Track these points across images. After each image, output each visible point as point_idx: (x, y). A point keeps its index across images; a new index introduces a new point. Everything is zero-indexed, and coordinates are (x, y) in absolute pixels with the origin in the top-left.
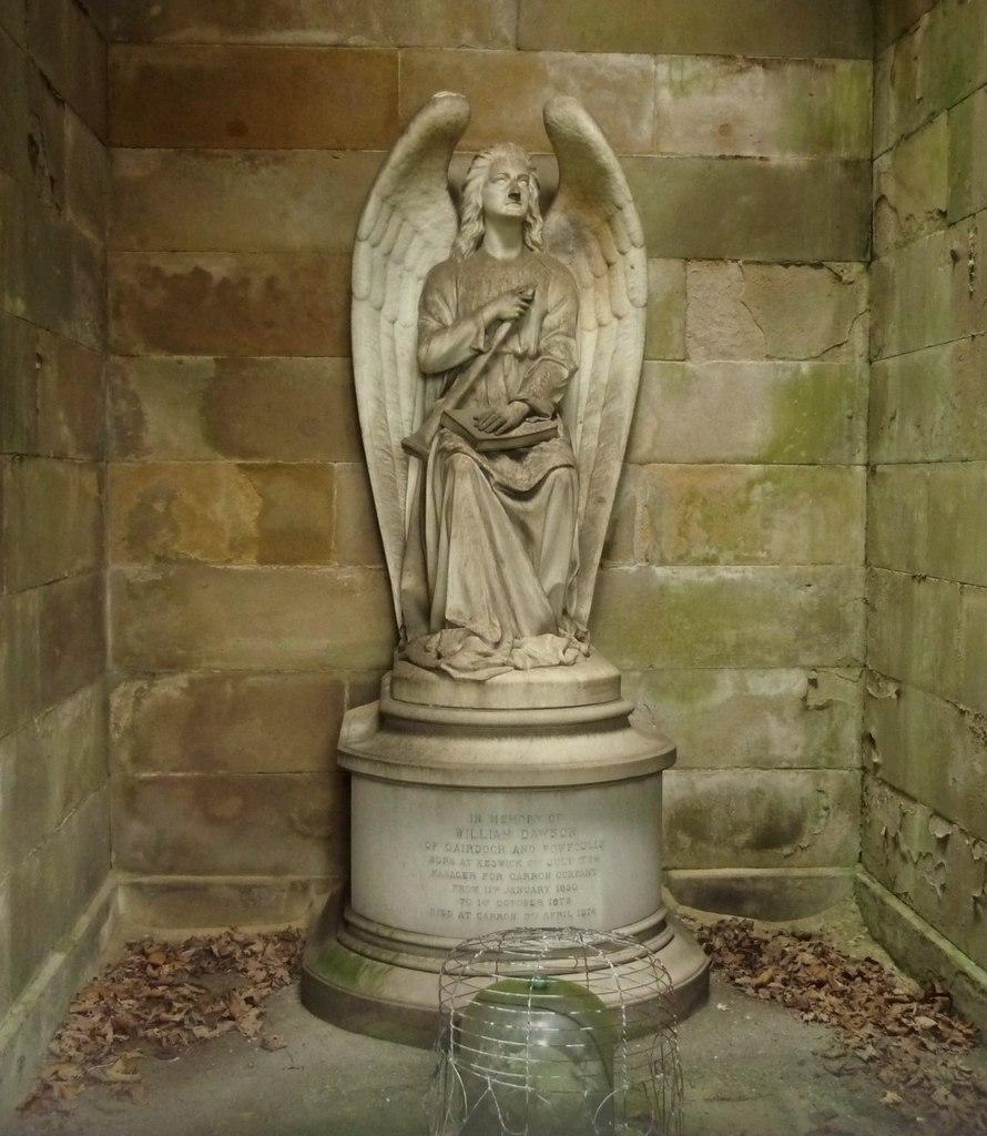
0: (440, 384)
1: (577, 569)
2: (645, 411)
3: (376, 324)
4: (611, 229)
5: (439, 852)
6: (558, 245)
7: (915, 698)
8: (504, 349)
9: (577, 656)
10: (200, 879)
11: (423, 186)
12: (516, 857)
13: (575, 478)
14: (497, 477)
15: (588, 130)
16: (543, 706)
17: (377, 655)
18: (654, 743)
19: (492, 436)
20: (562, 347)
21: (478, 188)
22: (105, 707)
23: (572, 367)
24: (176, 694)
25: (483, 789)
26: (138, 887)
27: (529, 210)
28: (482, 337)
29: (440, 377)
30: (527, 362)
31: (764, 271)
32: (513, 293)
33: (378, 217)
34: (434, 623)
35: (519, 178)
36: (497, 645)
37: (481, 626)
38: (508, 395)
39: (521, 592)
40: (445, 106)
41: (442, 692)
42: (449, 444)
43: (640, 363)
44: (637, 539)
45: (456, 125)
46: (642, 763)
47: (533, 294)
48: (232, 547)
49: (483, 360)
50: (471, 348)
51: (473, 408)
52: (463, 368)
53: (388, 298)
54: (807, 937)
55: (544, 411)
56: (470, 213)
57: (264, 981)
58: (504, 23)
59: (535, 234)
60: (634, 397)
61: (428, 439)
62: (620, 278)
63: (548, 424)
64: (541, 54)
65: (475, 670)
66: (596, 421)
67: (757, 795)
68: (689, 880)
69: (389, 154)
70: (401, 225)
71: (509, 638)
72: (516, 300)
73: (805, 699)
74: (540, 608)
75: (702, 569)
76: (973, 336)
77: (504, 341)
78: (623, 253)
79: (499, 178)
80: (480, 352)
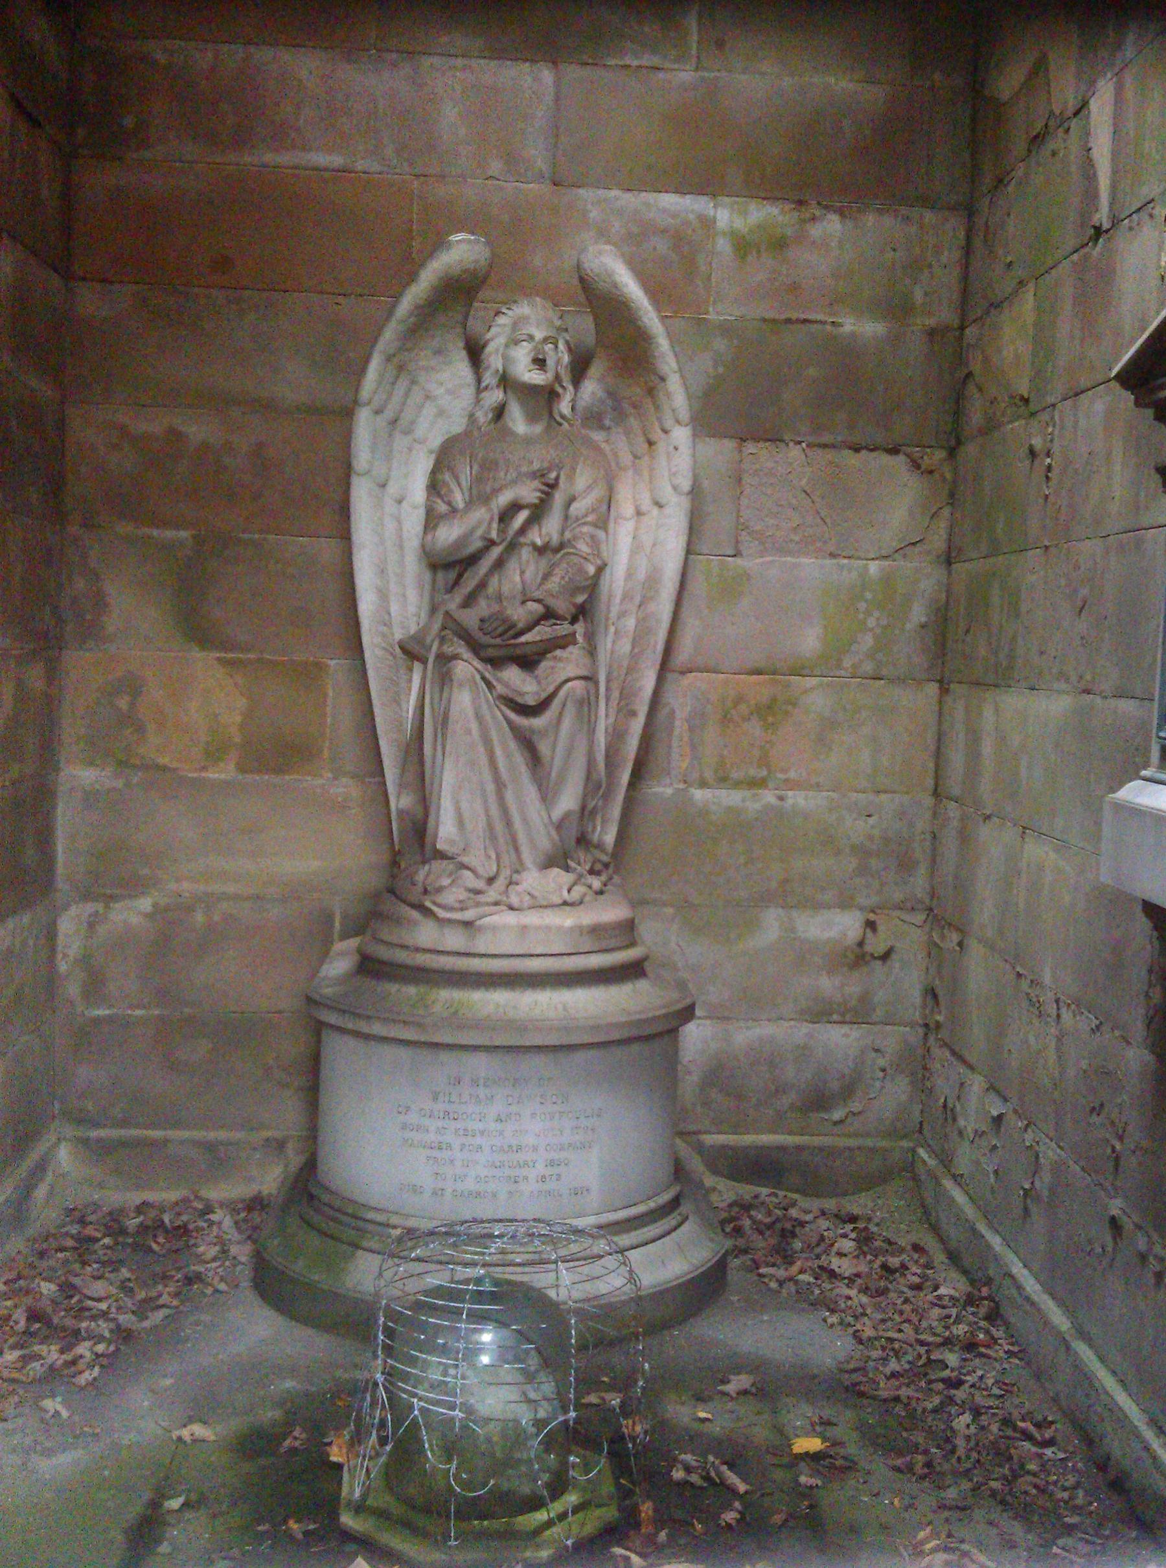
0: (452, 575)
1: (596, 789)
2: (686, 612)
3: (379, 505)
4: (654, 404)
5: (413, 1118)
6: (594, 419)
7: (976, 950)
8: (522, 540)
9: (585, 895)
10: (158, 1134)
11: (435, 343)
12: (500, 1126)
13: (592, 692)
14: (500, 689)
15: (627, 285)
16: (538, 952)
17: (375, 880)
18: (675, 995)
19: (498, 641)
20: (588, 540)
21: (497, 350)
22: (51, 934)
23: (599, 562)
24: (134, 920)
25: (464, 1048)
26: (85, 1142)
27: (557, 378)
28: (495, 525)
29: (451, 568)
30: (549, 555)
31: (830, 455)
32: (534, 475)
33: (381, 376)
34: (428, 854)
35: (546, 340)
36: (491, 880)
37: (473, 859)
38: (524, 592)
39: (525, 820)
40: (462, 251)
41: (425, 934)
42: (448, 649)
43: (682, 558)
44: (677, 755)
45: (474, 273)
46: (655, 1019)
47: (557, 479)
48: (207, 753)
49: (496, 552)
50: (484, 538)
51: (483, 608)
52: (473, 560)
53: (393, 474)
54: (853, 1219)
55: (561, 612)
56: (489, 379)
57: (214, 1259)
58: (537, 154)
59: (564, 407)
60: (673, 597)
61: (428, 640)
62: (662, 461)
63: (564, 629)
64: (581, 191)
65: (462, 909)
66: (630, 623)
67: (803, 1052)
68: (724, 1147)
69: (394, 306)
70: (410, 390)
71: (506, 873)
72: (536, 484)
73: (861, 944)
74: (545, 841)
75: (748, 794)
76: (1047, 547)
77: (523, 531)
78: (666, 432)
79: (523, 338)
80: (492, 543)
